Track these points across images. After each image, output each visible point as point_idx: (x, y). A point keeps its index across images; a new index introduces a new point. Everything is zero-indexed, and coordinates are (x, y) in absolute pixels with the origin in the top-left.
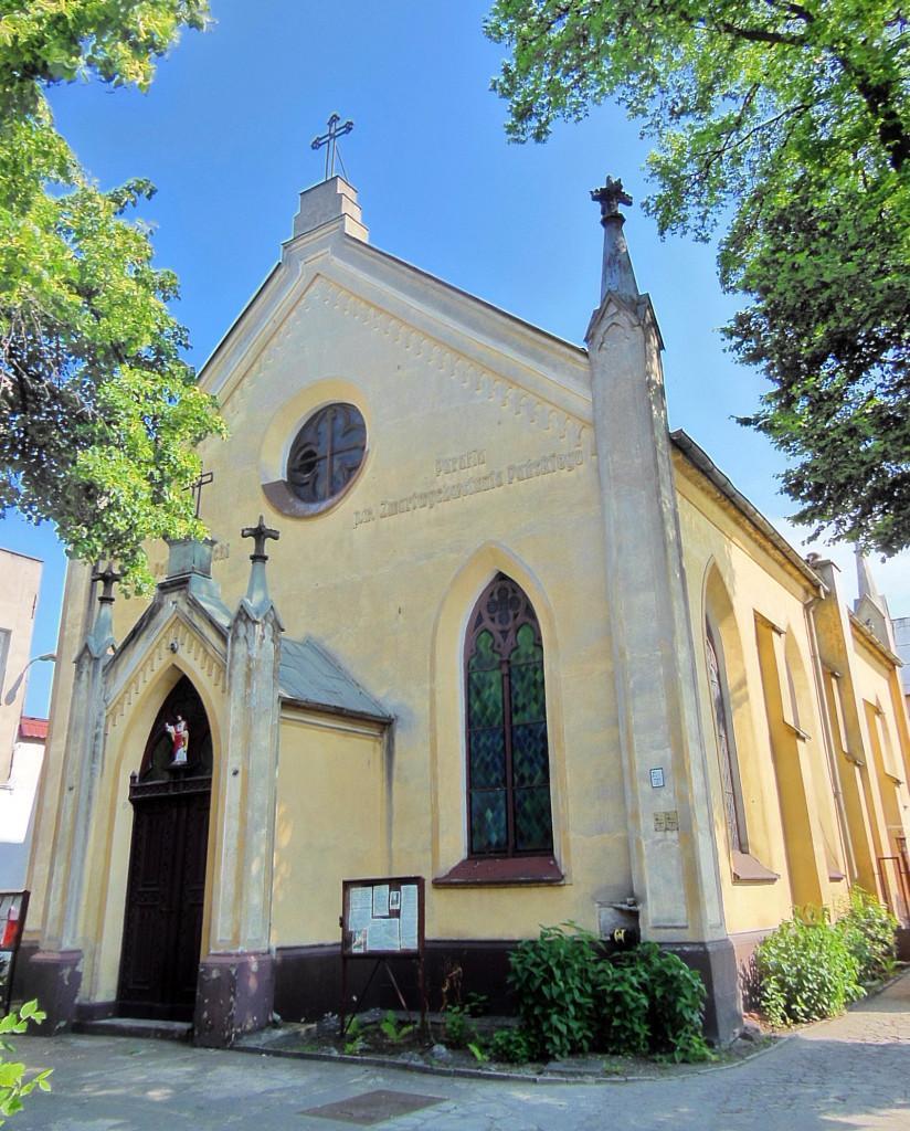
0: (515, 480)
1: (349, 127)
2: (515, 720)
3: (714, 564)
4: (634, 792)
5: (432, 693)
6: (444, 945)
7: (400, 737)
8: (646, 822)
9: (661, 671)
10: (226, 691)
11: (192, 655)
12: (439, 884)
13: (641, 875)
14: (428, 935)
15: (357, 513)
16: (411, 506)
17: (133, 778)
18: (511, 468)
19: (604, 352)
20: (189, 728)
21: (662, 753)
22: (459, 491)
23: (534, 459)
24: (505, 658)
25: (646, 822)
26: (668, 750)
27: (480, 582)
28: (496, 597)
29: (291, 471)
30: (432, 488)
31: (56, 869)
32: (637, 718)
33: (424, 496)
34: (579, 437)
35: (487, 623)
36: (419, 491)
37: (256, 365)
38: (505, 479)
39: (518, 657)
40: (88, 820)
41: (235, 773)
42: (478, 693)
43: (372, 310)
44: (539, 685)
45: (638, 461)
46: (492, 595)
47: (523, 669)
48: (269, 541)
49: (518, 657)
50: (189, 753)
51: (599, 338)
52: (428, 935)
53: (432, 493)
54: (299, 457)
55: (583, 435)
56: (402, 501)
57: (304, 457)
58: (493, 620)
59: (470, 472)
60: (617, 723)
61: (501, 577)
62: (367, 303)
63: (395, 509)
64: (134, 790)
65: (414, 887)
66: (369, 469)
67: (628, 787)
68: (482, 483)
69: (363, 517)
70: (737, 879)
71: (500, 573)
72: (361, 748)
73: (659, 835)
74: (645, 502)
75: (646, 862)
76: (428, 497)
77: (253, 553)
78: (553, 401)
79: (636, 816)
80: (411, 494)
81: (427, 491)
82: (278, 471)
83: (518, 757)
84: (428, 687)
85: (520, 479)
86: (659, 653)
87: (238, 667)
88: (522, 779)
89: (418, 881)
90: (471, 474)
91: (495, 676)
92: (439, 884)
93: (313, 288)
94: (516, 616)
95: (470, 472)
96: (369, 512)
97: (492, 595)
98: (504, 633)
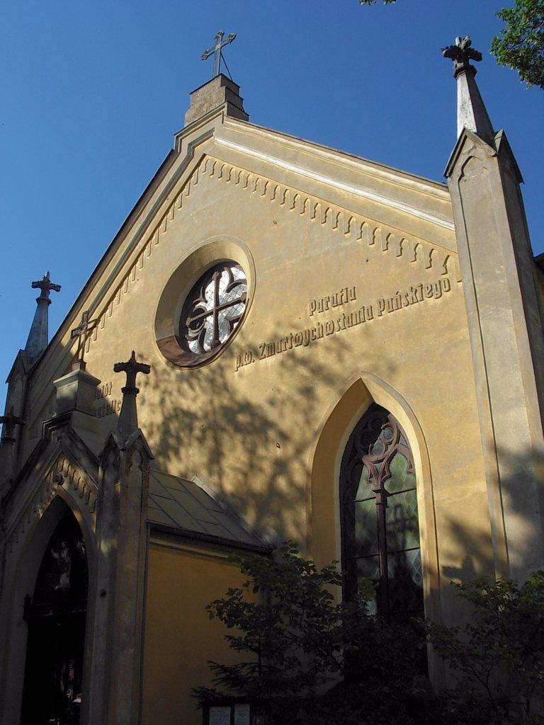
17: (27, 599)
41: (103, 594)
72: (471, 159)
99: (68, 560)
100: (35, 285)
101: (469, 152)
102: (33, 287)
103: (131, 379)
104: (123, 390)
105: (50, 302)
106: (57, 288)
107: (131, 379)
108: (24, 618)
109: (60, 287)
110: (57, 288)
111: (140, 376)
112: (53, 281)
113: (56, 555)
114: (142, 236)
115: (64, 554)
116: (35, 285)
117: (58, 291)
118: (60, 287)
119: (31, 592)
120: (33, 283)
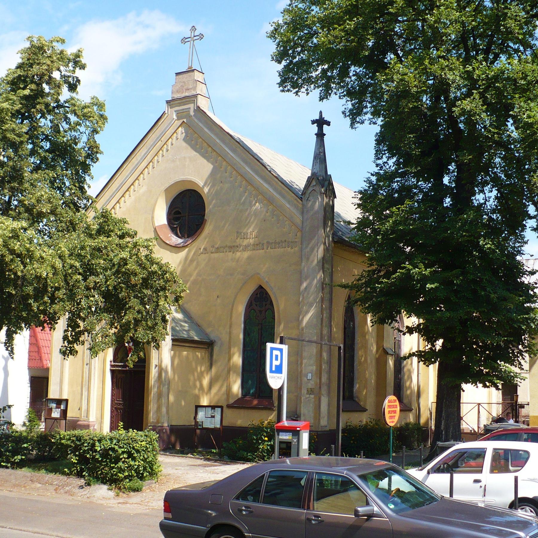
0: (269, 248)
4: (301, 380)
5: (230, 333)
6: (326, 433)
7: (216, 349)
8: (304, 391)
12: (229, 406)
13: (300, 410)
14: (224, 424)
16: (225, 250)
18: (268, 243)
21: (312, 368)
23: (277, 241)
25: (304, 391)
26: (314, 367)
27: (251, 289)
28: (258, 296)
30: (234, 244)
31: (58, 388)
32: (305, 354)
33: (231, 247)
36: (229, 244)
38: (265, 247)
40: (94, 376)
42: (249, 335)
43: (210, 149)
46: (257, 294)
51: (307, 195)
52: (224, 424)
54: (173, 212)
55: (298, 234)
57: (175, 213)
58: (256, 305)
61: (261, 287)
62: (208, 145)
63: (218, 250)
65: (220, 409)
67: (299, 379)
70: (343, 411)
71: (260, 286)
73: (308, 396)
75: (302, 404)
79: (301, 389)
84: (228, 331)
85: (271, 248)
89: (222, 407)
92: (229, 406)
94: (266, 305)
97: (257, 294)
98: (261, 312)
100: (313, 122)
103: (320, 128)
104: (316, 134)
106: (328, 123)
111: (325, 126)
116: (313, 122)
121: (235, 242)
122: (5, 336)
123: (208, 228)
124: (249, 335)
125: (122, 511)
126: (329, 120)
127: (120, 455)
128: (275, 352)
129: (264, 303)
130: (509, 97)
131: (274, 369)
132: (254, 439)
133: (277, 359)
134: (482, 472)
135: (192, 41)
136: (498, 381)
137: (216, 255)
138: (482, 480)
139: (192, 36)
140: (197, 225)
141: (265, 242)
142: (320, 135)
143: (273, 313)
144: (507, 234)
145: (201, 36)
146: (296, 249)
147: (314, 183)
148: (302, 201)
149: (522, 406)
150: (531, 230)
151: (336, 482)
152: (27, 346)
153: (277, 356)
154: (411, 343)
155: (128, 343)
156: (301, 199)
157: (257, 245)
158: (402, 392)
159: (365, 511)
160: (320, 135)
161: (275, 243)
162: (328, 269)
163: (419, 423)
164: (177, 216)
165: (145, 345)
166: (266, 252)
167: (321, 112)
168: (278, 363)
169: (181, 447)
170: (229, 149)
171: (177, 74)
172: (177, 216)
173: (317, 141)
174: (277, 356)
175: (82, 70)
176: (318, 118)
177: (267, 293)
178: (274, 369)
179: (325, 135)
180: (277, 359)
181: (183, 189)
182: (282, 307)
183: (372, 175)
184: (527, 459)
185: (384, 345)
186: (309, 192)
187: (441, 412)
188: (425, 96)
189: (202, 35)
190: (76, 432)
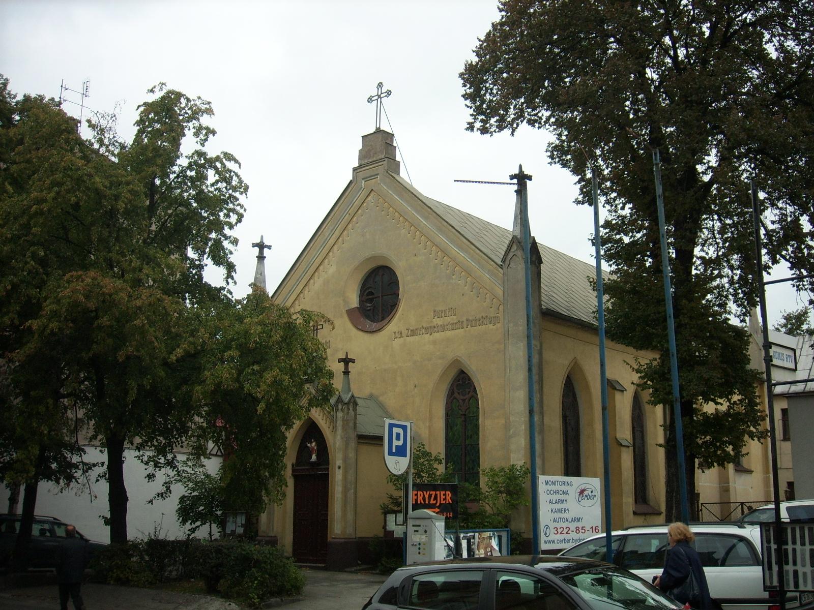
0: (469, 326)
1: (389, 93)
2: (467, 442)
3: (576, 362)
9: (523, 428)
10: (334, 430)
11: (318, 413)
15: (395, 333)
17: (293, 465)
19: (509, 269)
20: (317, 445)
22: (443, 328)
24: (464, 413)
29: (361, 302)
30: (431, 325)
33: (427, 328)
34: (498, 309)
35: (456, 395)
37: (341, 239)
39: (469, 412)
41: (339, 468)
42: (451, 429)
44: (477, 426)
45: (521, 328)
47: (471, 418)
48: (350, 364)
49: (469, 412)
50: (317, 456)
51: (507, 262)
53: (430, 327)
54: (365, 294)
56: (416, 330)
58: (459, 393)
59: (448, 319)
60: (695, 337)
63: (413, 333)
64: (293, 470)
65: (794, 368)
66: (400, 310)
68: (454, 326)
69: (398, 336)
72: (515, 256)
74: (522, 348)
76: (430, 330)
77: (343, 370)
78: (488, 288)
80: (421, 326)
81: (428, 325)
82: (354, 302)
83: (468, 459)
86: (523, 419)
87: (338, 422)
88: (469, 468)
90: (449, 320)
91: (459, 421)
93: (370, 198)
95: (448, 319)
96: (401, 333)
99: (315, 448)
100: (254, 245)
101: (514, 252)
102: (253, 247)
103: (261, 252)
104: (257, 257)
105: (265, 257)
106: (269, 247)
107: (261, 252)
108: (292, 475)
109: (271, 246)
110: (269, 247)
111: (266, 250)
112: (266, 243)
113: (309, 445)
114: (669, 483)
115: (313, 444)
116: (254, 245)
117: (270, 249)
118: (271, 246)
119: (295, 462)
120: (253, 244)
121: (432, 322)
122: (203, 275)
123: (394, 325)
124: (451, 429)
125: (336, 506)
126: (529, 174)
127: (789, 16)
128: (396, 430)
129: (467, 390)
130: (33, 481)
131: (394, 450)
132: (810, 75)
133: (398, 438)
134: (363, 137)
135: (379, 94)
136: (30, 321)
137: (411, 339)
138: (151, 483)
139: (379, 94)
140: (391, 306)
141: (464, 319)
142: (261, 258)
143: (477, 400)
144: (546, 19)
145: (389, 93)
146: (499, 325)
147: (515, 247)
148: (502, 268)
149: (47, 481)
150: (213, 114)
151: (654, 72)
152: (789, 419)
153: (398, 435)
154: (172, 176)
155: (94, 279)
156: (501, 267)
157: (456, 323)
158: (647, 492)
159: (788, 580)
160: (261, 258)
161: (476, 320)
162: (536, 346)
163: (264, 293)
164: (370, 297)
165: (151, 469)
166: (466, 331)
167: (520, 167)
168: (400, 443)
169: (585, 192)
170: (310, 563)
171: (455, 181)
172: (370, 297)
173: (517, 199)
174: (398, 435)
175: (464, 112)
176: (344, 357)
177: (470, 379)
178: (394, 450)
179: (265, 257)
180: (398, 438)
181: (381, 263)
182: (474, 368)
183: (179, 519)
184: (473, 76)
185: (617, 436)
186: (509, 257)
187: (672, 508)
188: (588, 163)
189: (369, 102)
190: (340, 428)
